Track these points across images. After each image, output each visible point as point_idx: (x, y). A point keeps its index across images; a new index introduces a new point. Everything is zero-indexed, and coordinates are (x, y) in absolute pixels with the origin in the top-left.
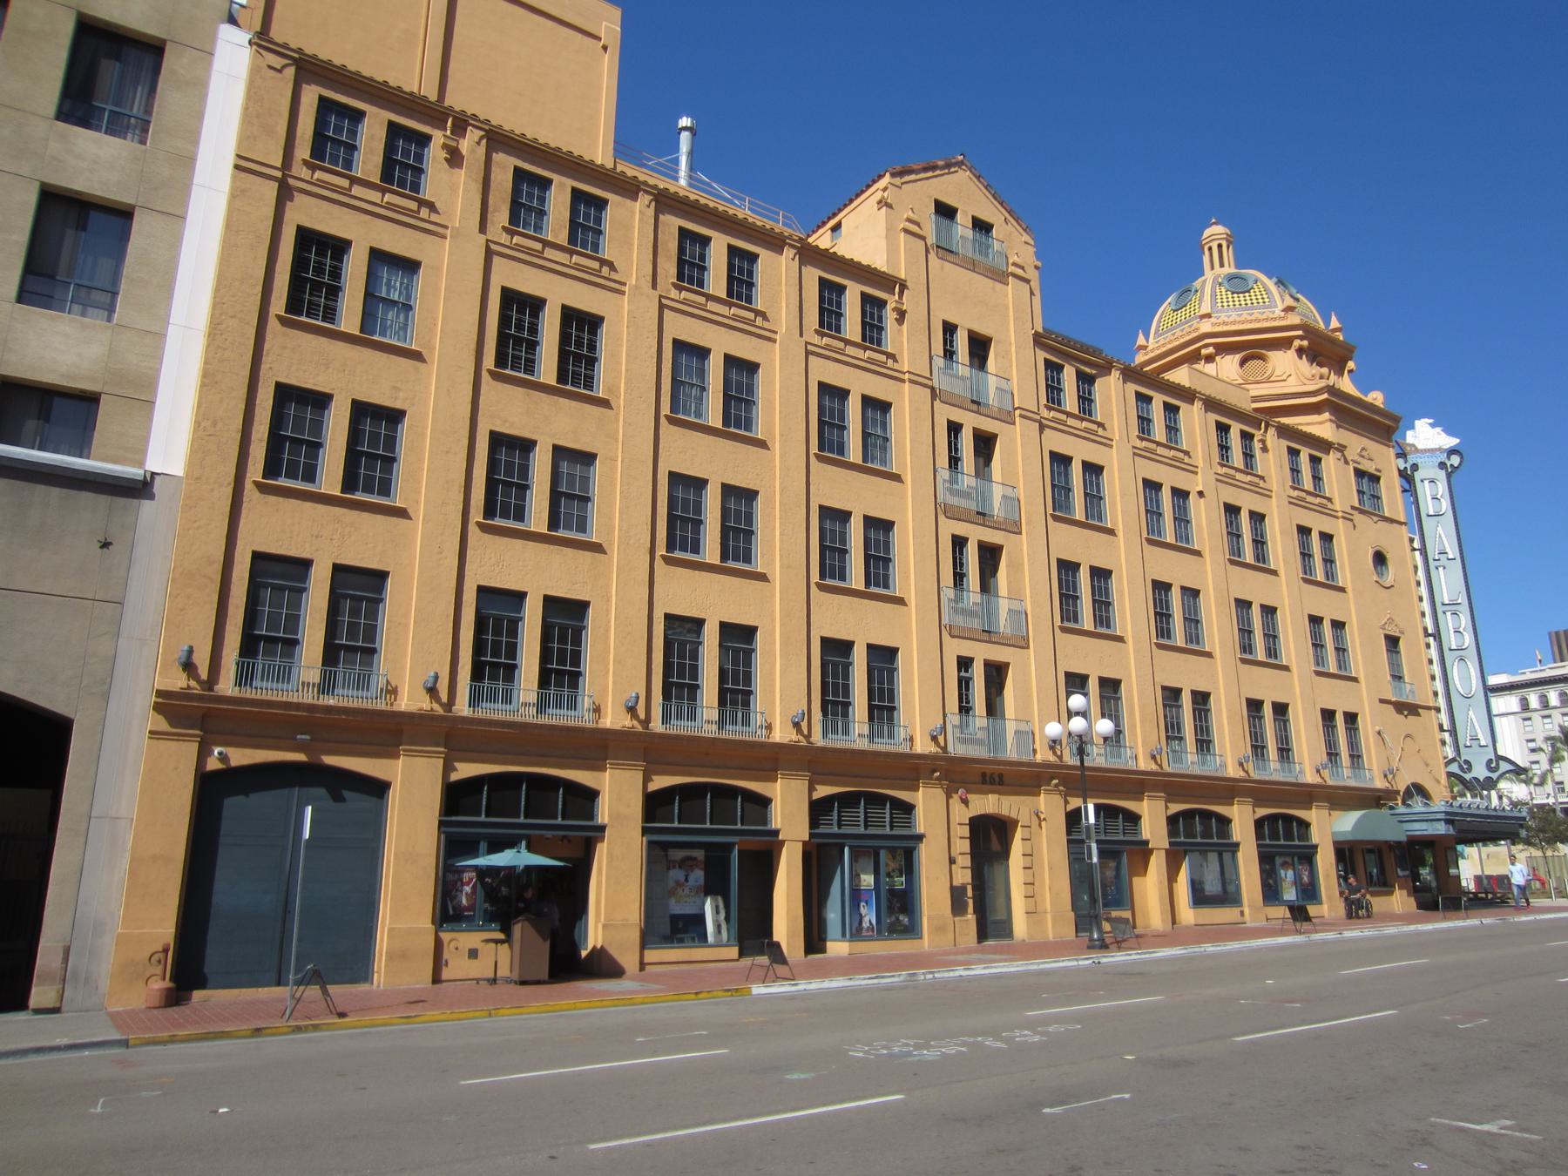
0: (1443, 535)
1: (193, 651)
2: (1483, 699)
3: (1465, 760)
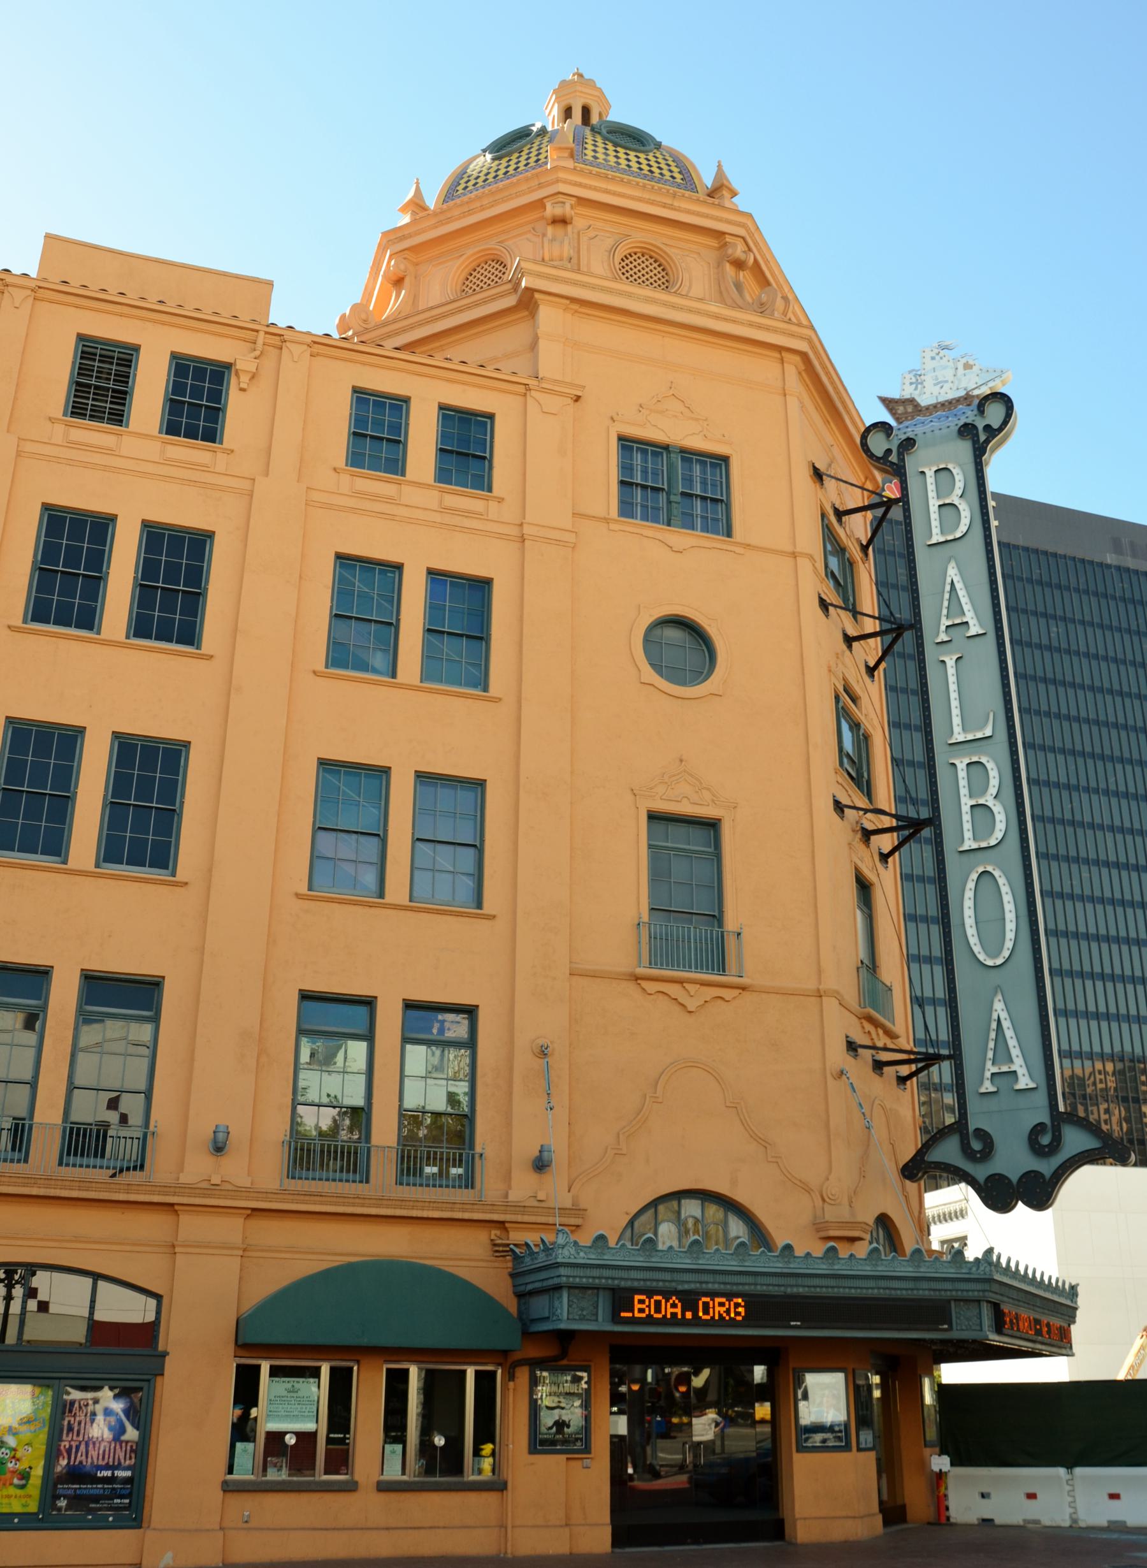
0: (959, 586)
1: (5, 1298)
2: (375, 1101)
3: (977, 1130)
